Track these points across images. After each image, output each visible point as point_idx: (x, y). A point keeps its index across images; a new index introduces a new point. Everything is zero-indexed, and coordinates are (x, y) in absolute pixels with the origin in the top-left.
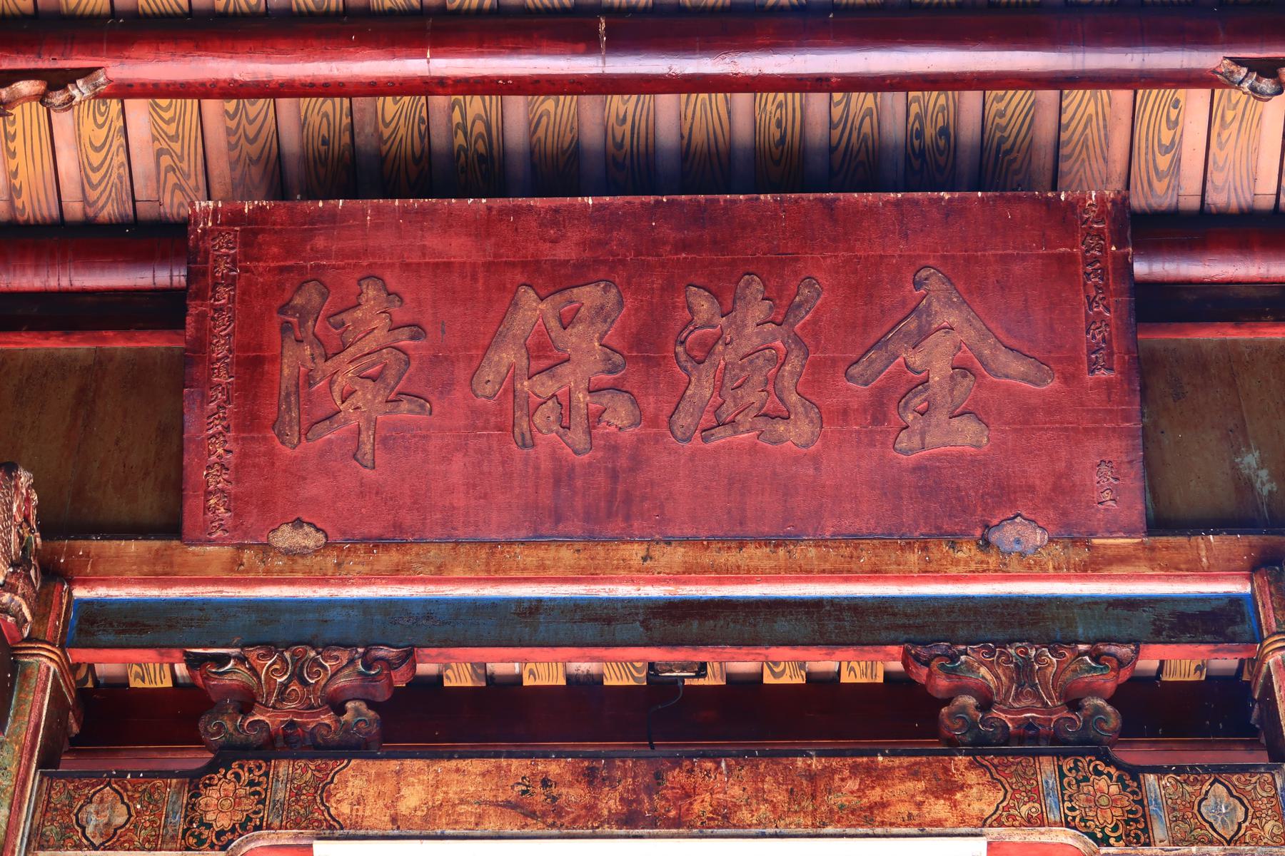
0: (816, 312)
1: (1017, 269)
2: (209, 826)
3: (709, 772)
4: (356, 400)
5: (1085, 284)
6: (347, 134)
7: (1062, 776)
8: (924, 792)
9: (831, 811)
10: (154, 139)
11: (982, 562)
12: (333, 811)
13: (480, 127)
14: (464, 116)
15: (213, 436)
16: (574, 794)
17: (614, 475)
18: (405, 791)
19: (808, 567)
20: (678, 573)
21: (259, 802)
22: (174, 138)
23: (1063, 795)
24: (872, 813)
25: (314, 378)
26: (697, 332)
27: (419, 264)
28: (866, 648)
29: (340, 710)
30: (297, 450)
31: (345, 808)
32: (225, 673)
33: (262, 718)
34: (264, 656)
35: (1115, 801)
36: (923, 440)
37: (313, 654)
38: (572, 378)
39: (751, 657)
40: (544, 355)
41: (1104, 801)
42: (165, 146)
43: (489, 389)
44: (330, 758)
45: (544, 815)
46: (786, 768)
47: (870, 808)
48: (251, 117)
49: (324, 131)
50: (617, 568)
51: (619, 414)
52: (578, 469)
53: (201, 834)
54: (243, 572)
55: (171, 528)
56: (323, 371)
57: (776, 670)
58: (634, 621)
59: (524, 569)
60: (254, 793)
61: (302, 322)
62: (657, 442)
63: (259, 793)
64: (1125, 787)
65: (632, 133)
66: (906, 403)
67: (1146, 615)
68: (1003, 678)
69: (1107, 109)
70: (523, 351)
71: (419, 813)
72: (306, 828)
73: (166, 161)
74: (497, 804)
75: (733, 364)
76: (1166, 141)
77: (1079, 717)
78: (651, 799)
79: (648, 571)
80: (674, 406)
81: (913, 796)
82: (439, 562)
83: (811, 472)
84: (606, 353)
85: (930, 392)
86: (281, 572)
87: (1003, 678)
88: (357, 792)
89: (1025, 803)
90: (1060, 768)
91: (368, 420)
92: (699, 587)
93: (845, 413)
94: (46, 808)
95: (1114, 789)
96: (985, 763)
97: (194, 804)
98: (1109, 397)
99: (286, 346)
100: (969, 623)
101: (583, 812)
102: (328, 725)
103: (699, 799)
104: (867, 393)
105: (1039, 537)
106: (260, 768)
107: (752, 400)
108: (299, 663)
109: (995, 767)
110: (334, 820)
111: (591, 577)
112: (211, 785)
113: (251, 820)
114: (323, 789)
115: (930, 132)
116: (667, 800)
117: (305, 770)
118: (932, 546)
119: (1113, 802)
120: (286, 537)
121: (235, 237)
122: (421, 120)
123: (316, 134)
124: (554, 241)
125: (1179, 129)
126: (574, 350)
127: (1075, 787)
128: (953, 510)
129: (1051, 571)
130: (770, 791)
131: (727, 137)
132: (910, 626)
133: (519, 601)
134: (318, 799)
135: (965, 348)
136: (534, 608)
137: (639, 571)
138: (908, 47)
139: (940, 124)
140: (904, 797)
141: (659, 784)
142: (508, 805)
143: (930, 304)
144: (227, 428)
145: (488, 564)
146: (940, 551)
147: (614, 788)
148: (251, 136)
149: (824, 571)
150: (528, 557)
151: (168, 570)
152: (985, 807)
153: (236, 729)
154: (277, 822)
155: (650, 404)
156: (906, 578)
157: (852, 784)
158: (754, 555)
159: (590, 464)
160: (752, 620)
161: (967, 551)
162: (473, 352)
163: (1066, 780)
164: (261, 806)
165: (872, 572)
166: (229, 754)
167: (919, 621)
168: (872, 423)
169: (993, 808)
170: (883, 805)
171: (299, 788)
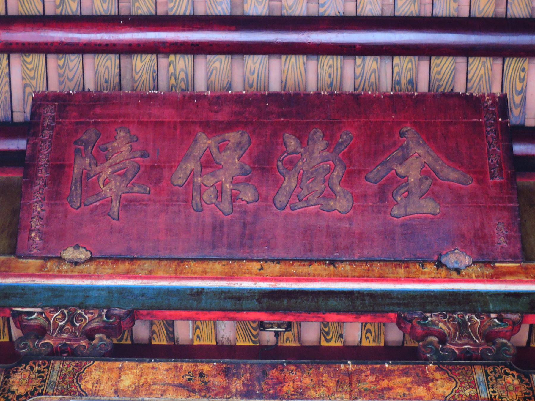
0: (350, 147)
1: (452, 128)
2: (13, 393)
3: (292, 371)
4: (112, 185)
5: (487, 136)
6: (118, 77)
7: (487, 375)
8: (412, 382)
9: (360, 391)
10: (23, 78)
11: (438, 274)
12: (82, 387)
13: (182, 75)
14: (175, 69)
15: (36, 202)
16: (218, 381)
17: (245, 225)
18: (123, 377)
20: (277, 276)
21: (42, 382)
22: (32, 78)
23: (488, 385)
24: (383, 393)
25: (90, 175)
26: (288, 156)
27: (147, 122)
28: (378, 314)
29: (92, 338)
30: (79, 210)
31: (90, 386)
32: (32, 319)
33: (49, 341)
34: (53, 311)
35: (517, 388)
36: (406, 210)
38: (223, 177)
39: (315, 319)
40: (209, 163)
41: (511, 388)
42: (28, 82)
43: (180, 182)
44: (83, 360)
45: (200, 391)
46: (335, 370)
47: (382, 390)
48: (71, 68)
50: (245, 273)
51: (248, 195)
52: (225, 222)
53: (8, 396)
54: (47, 271)
56: (95, 171)
57: (328, 338)
58: (253, 299)
59: (195, 273)
60: (40, 377)
61: (86, 148)
62: (267, 209)
63: (43, 377)
64: (522, 381)
65: (258, 79)
66: (397, 192)
67: (525, 300)
68: (452, 329)
69: (490, 72)
70: (199, 163)
71: (130, 389)
72: (66, 395)
73: (28, 90)
74: (174, 385)
75: (307, 171)
76: (519, 88)
78: (260, 385)
79: (261, 274)
81: (405, 385)
82: (150, 269)
84: (241, 165)
85: (409, 186)
86: (67, 272)
87: (452, 329)
88: (97, 377)
89: (468, 389)
90: (486, 371)
91: (117, 195)
92: (288, 283)
93: (365, 196)
95: (516, 382)
96: (444, 368)
97: (7, 381)
98: (501, 190)
100: (432, 303)
101: (222, 390)
103: (287, 384)
105: (467, 260)
106: (44, 364)
107: (317, 189)
109: (450, 370)
110: (82, 391)
111: (231, 277)
112: (16, 372)
113: (37, 390)
114: (78, 376)
115: (404, 82)
116: (269, 385)
117: (69, 366)
118: (411, 266)
119: (516, 389)
120: (69, 254)
121: (55, 108)
122: (154, 71)
123: (102, 78)
124: (216, 112)
125: (525, 82)
127: (494, 381)
129: (474, 278)
130: (326, 381)
131: (304, 83)
132: (400, 304)
133: (192, 289)
134: (75, 381)
135: (426, 166)
136: (200, 292)
137: (256, 275)
138: (394, 31)
139: (409, 78)
140: (400, 385)
141: (264, 377)
142: (180, 386)
143: (408, 144)
145: (176, 270)
146: (414, 268)
147: (239, 378)
148: (70, 78)
149: (354, 276)
150: (198, 267)
151: (7, 270)
152: (446, 391)
153: (34, 346)
154: (51, 392)
155: (264, 190)
156: (398, 280)
157: (372, 378)
158: (317, 268)
159: (232, 220)
160: (316, 300)
161: (430, 268)
162: (173, 164)
163: (489, 377)
164: (43, 383)
165: (379, 277)
167: (405, 301)
169: (450, 391)
170: (389, 389)
171: (65, 375)
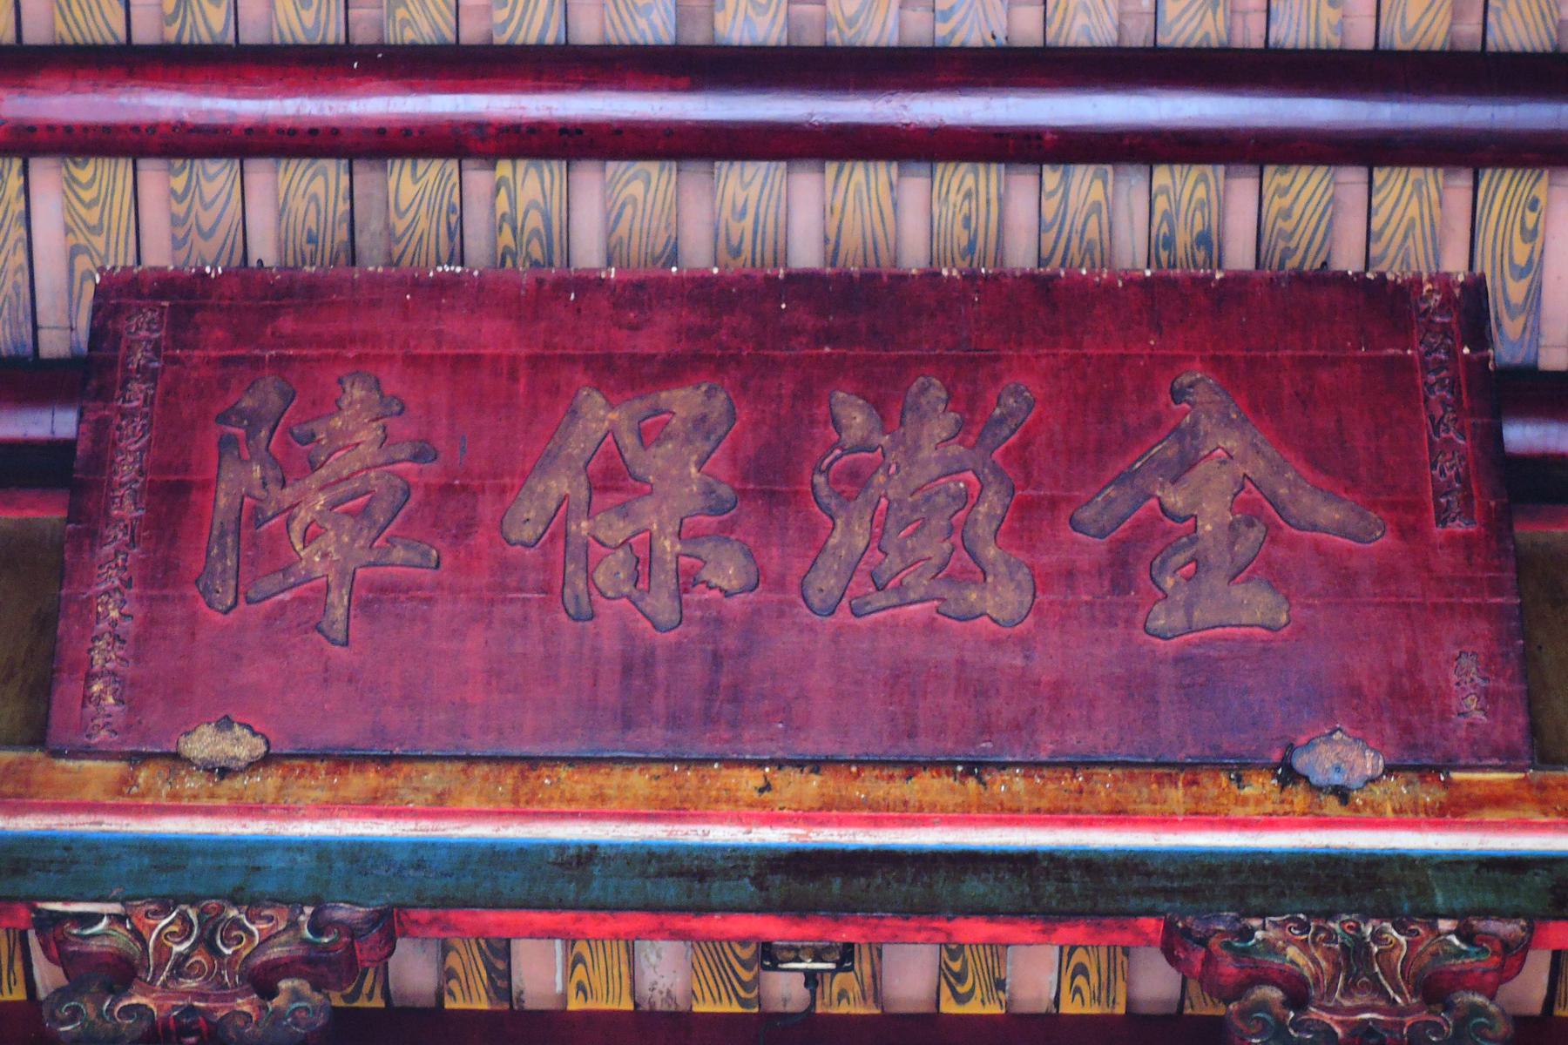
0: (1026, 432)
1: (1325, 376)
4: (328, 542)
5: (1426, 399)
10: (68, 230)
11: (1282, 802)
13: (535, 221)
14: (513, 202)
15: (106, 592)
17: (717, 659)
19: (1015, 805)
20: (811, 809)
22: (96, 230)
25: (263, 512)
27: (431, 356)
28: (1107, 921)
29: (269, 992)
30: (231, 615)
32: (93, 936)
34: (155, 913)
36: (1189, 615)
37: (233, 913)
38: (654, 518)
39: (924, 935)
40: (611, 479)
42: (82, 241)
43: (528, 533)
48: (208, 199)
49: (311, 222)
50: (717, 801)
51: (726, 570)
52: (659, 652)
54: (136, 795)
56: (278, 502)
57: (961, 989)
58: (740, 877)
59: (570, 801)
61: (251, 433)
62: (781, 614)
65: (755, 233)
66: (1163, 562)
67: (1540, 879)
68: (1324, 964)
69: (1436, 211)
70: (583, 478)
75: (900, 501)
76: (1521, 259)
79: (764, 805)
80: (809, 562)
82: (439, 789)
83: (1019, 662)
84: (708, 484)
85: (1199, 546)
86: (195, 797)
87: (1324, 964)
91: (342, 573)
92: (843, 831)
93: (1069, 574)
98: (1468, 558)
99: (224, 466)
100: (1265, 888)
102: (249, 1016)
104: (1104, 547)
105: (1370, 763)
107: (928, 553)
111: (676, 813)
115: (1183, 239)
118: (1205, 779)
120: (203, 743)
121: (161, 315)
122: (451, 209)
124: (634, 328)
125: (1539, 241)
126: (660, 477)
129: (1390, 814)
132: (1173, 890)
133: (562, 847)
135: (1249, 485)
136: (585, 857)
137: (750, 806)
138: (1154, 90)
139: (1198, 228)
143: (1195, 423)
144: (127, 583)
145: (515, 791)
146: (1214, 786)
148: (206, 228)
149: (1038, 810)
150: (581, 783)
151: (22, 790)
153: (100, 1015)
155: (774, 559)
156: (1166, 821)
158: (930, 787)
159: (679, 644)
160: (926, 879)
161: (1259, 786)
162: (507, 480)
165: (1112, 812)
168: (1112, 592)
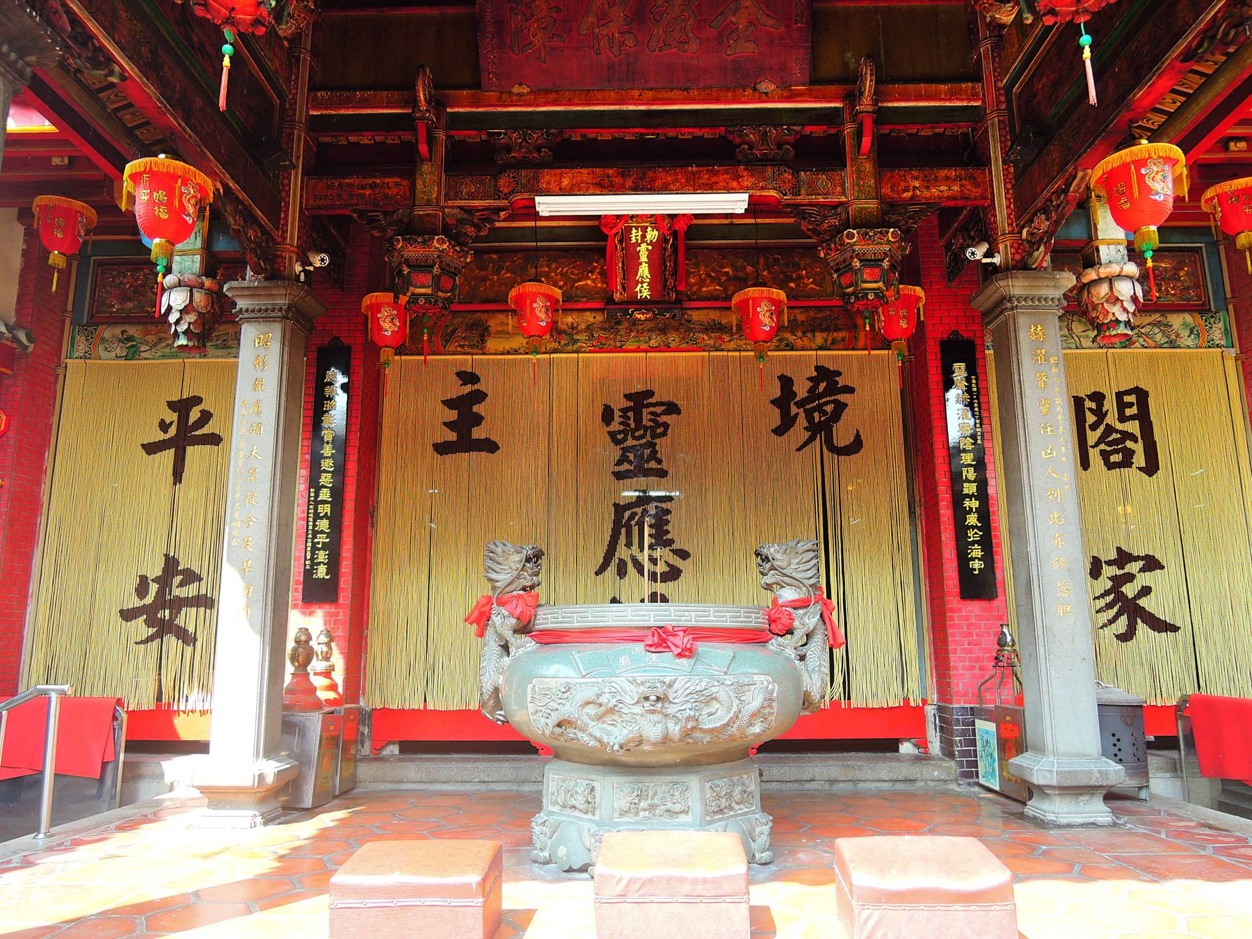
16: (618, 180)
55: (476, 85)
77: (781, 152)
94: (448, 186)
105: (773, 87)
108: (525, 134)
120: (516, 89)
128: (743, 78)
150: (599, 95)
166: (505, 168)
170: (716, 183)
